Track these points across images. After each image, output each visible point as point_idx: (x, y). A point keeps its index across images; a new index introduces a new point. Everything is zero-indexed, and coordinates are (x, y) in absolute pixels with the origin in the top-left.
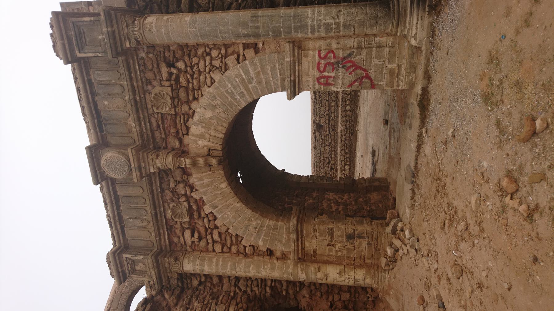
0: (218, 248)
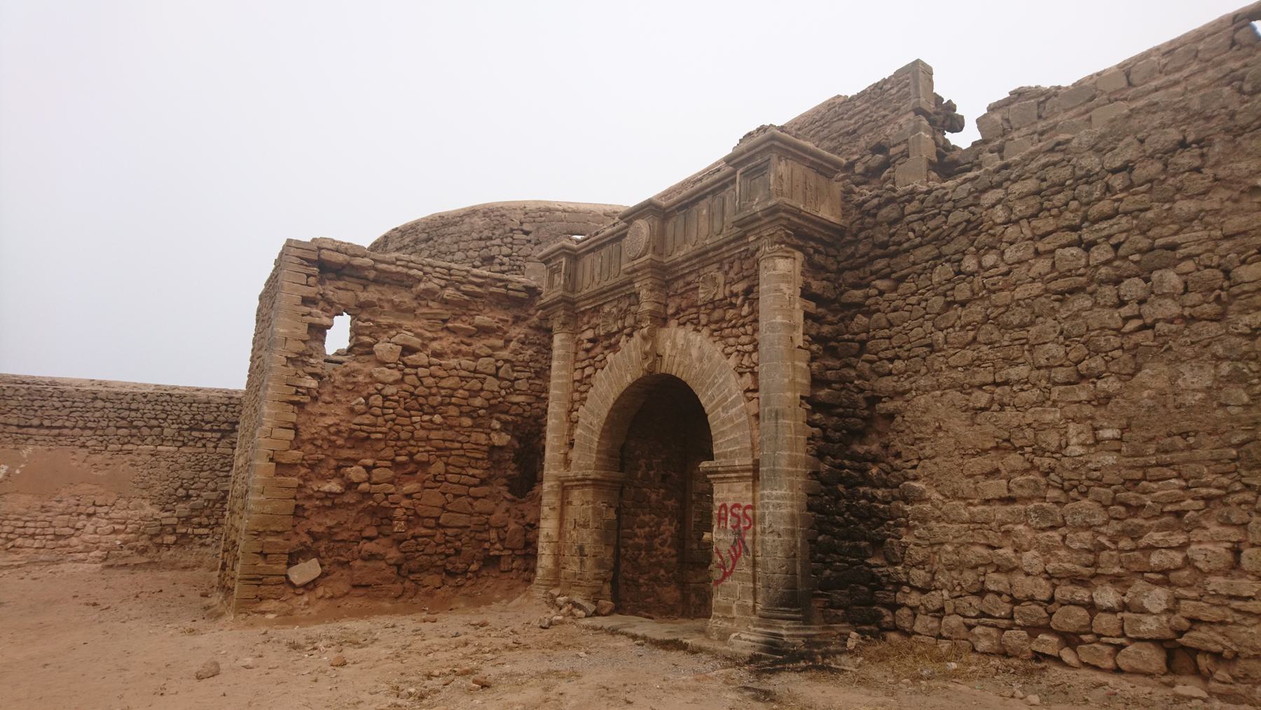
0: (577, 376)
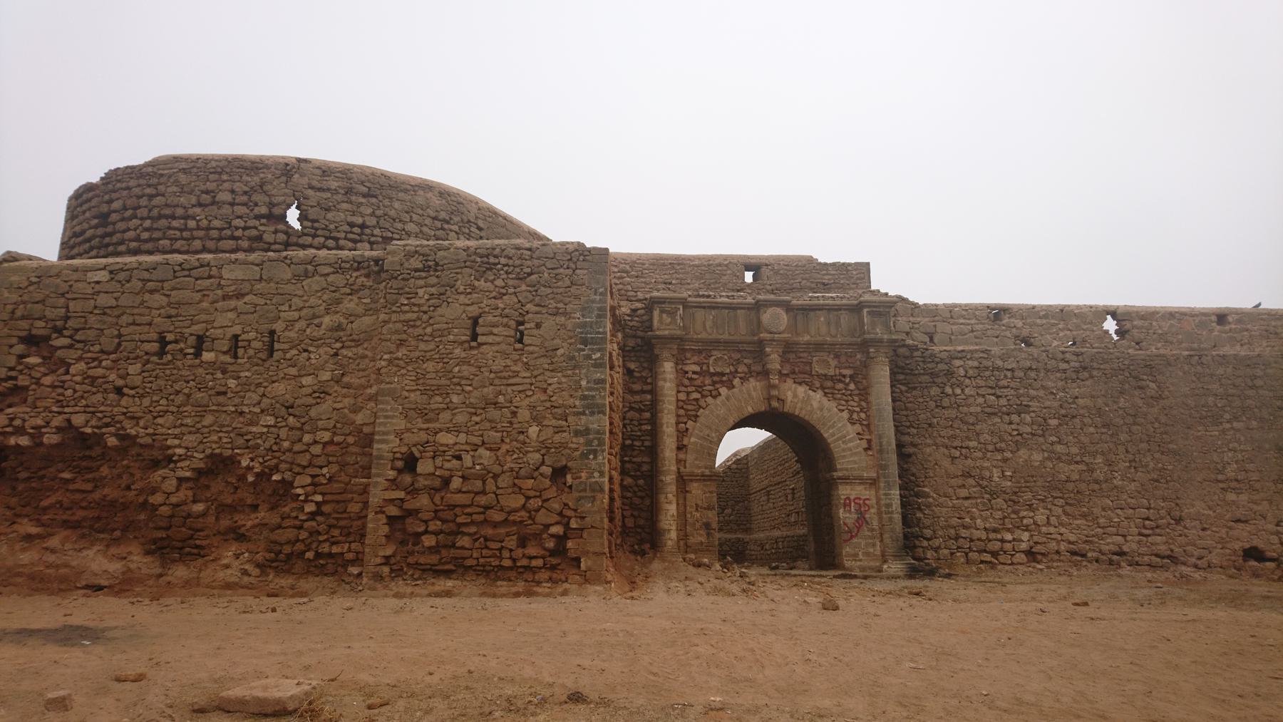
0: (682, 396)
